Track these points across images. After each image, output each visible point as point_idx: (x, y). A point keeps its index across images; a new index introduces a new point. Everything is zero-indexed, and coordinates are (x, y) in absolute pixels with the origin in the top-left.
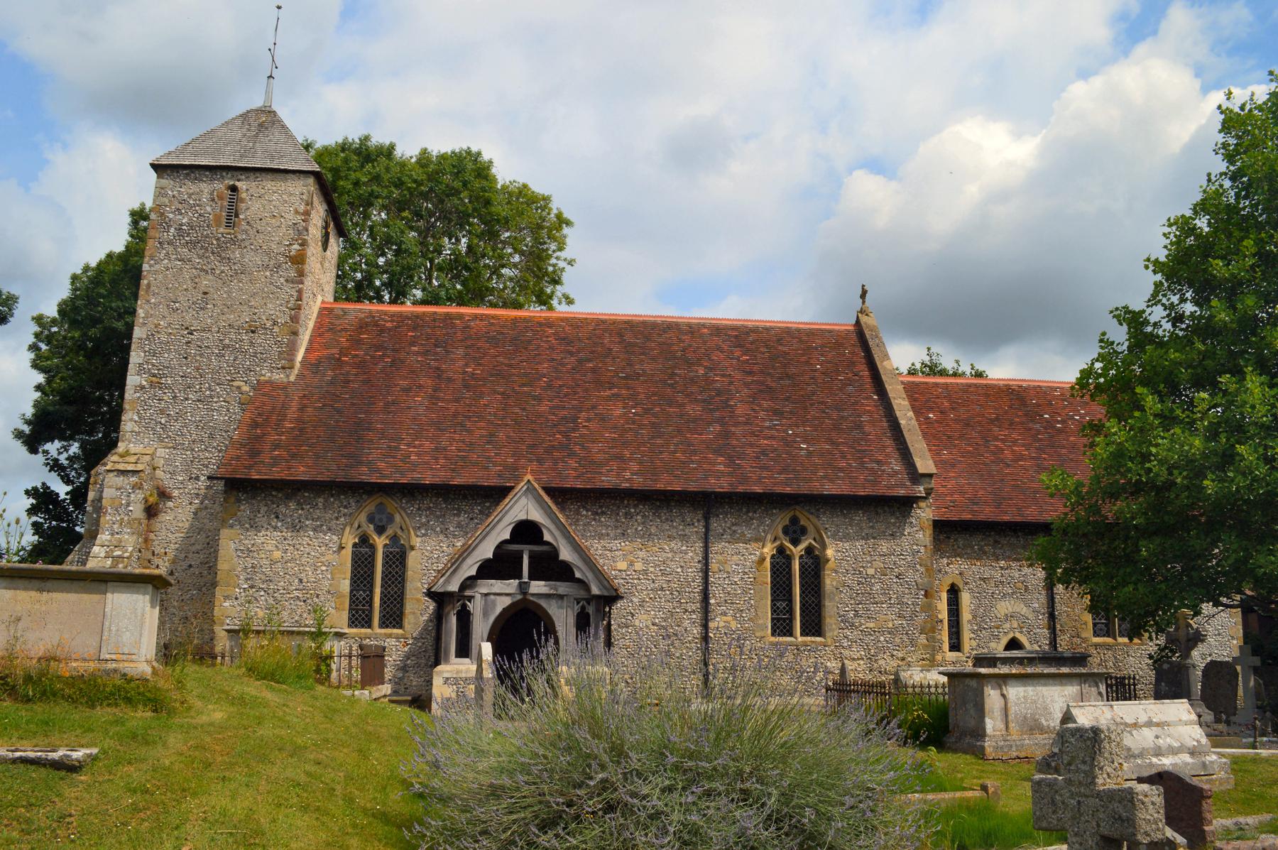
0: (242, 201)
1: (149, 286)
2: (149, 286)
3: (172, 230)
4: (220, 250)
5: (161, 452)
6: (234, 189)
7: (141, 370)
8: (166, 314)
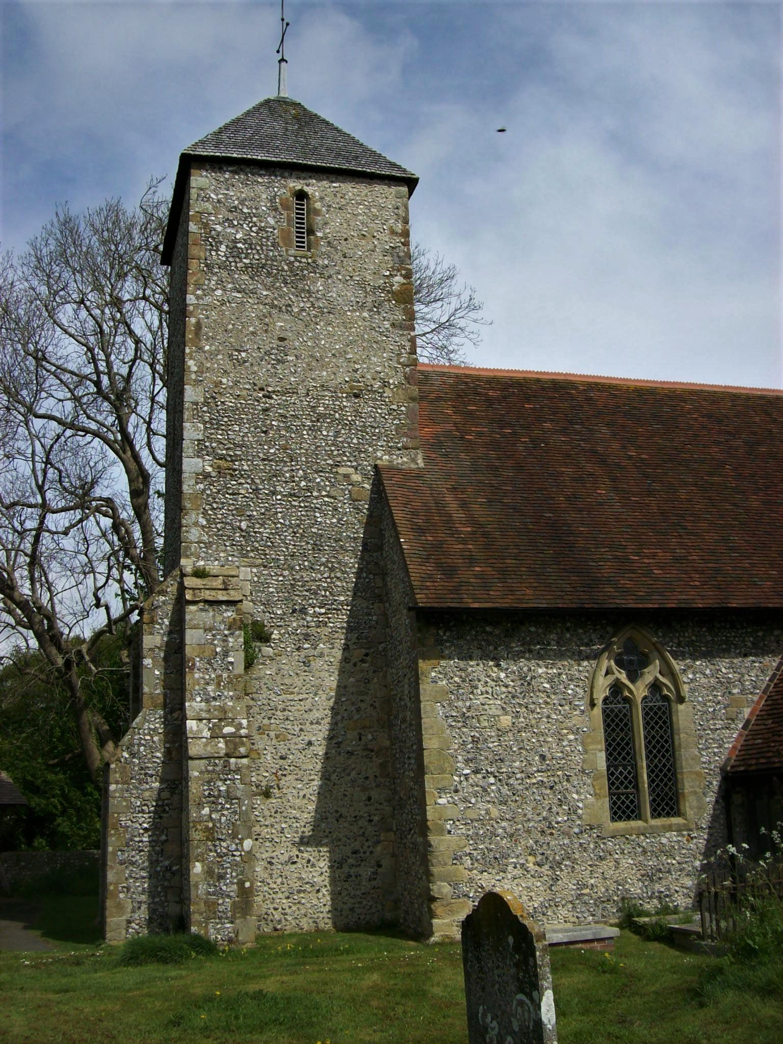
0: (317, 212)
1: (198, 325)
2: (198, 325)
3: (223, 248)
4: (296, 278)
5: (246, 573)
6: (301, 196)
7: (201, 450)
8: (229, 367)
